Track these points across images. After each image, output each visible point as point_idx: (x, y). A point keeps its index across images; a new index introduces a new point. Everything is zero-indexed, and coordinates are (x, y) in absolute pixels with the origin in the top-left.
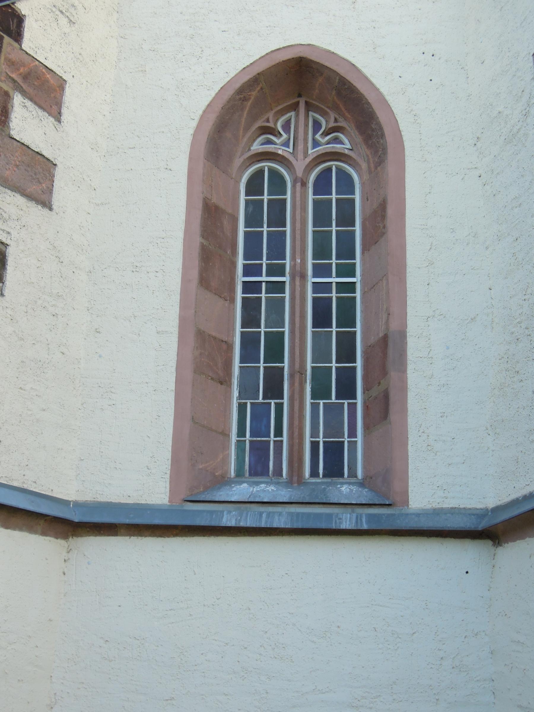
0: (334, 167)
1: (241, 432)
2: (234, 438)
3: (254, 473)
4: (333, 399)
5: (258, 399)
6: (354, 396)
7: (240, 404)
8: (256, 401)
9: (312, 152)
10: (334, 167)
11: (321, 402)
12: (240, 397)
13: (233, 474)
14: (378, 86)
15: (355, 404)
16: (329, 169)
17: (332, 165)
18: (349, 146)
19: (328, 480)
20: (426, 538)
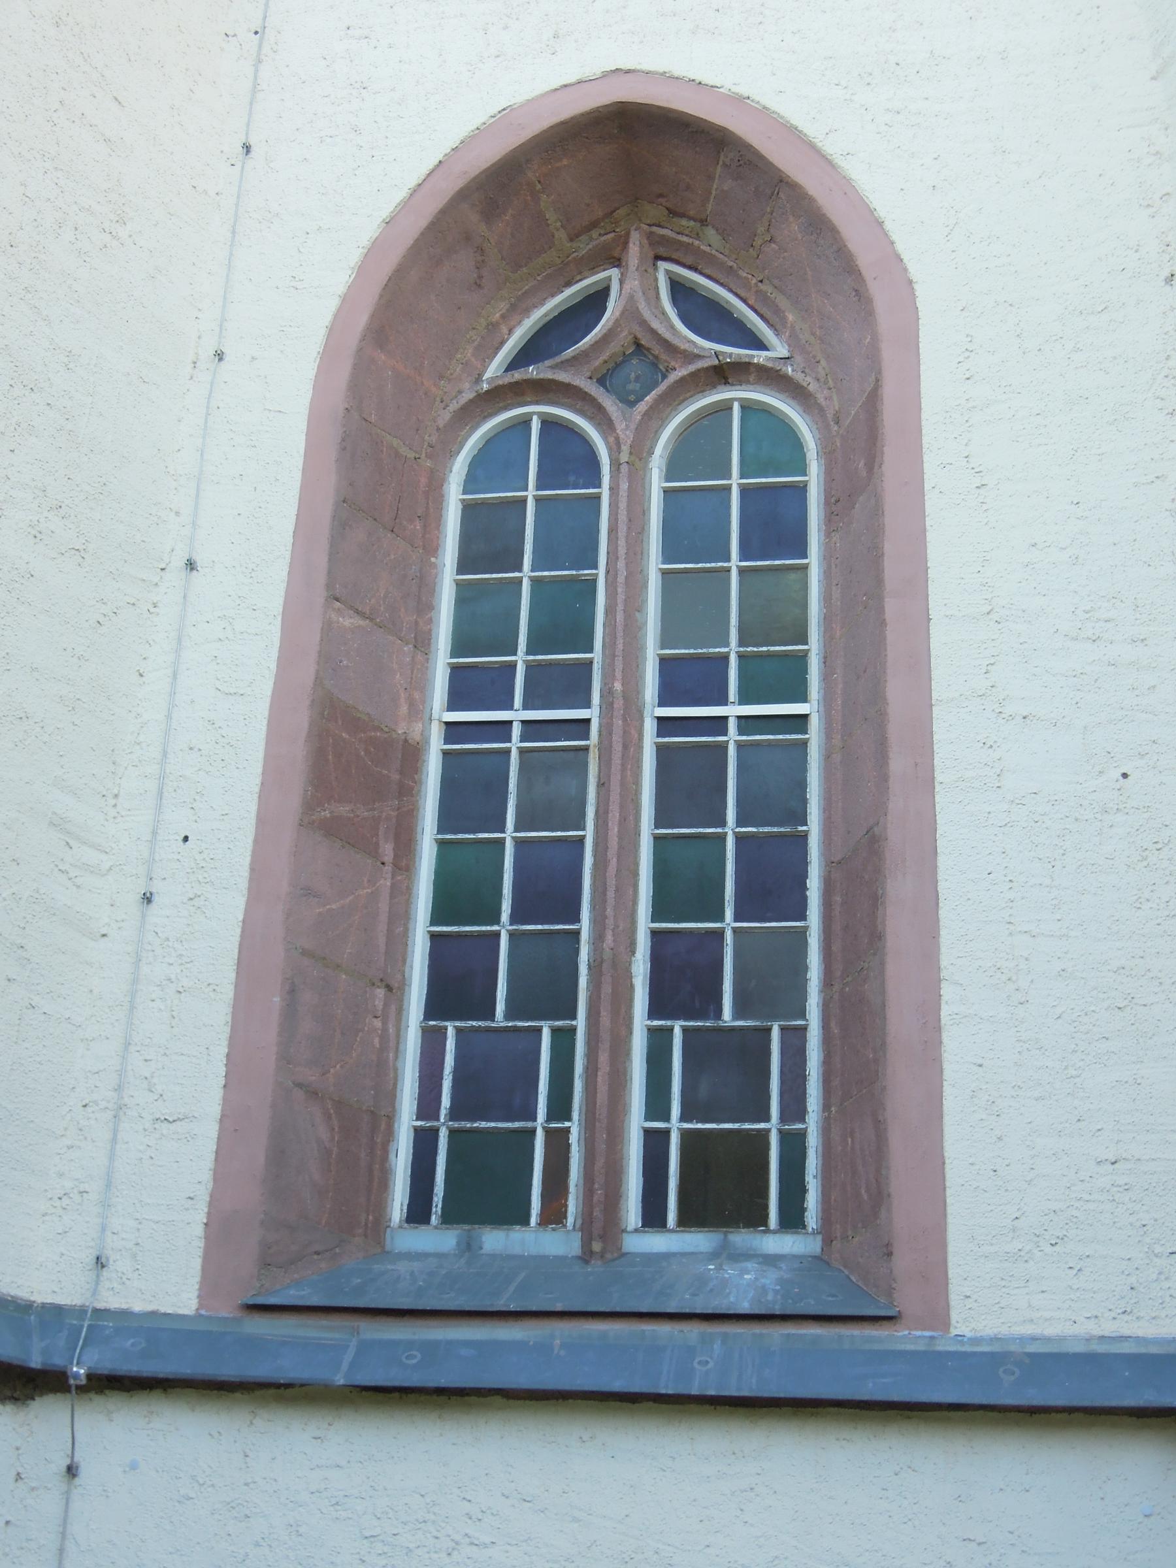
1: (427, 1105)
16: (525, 422)
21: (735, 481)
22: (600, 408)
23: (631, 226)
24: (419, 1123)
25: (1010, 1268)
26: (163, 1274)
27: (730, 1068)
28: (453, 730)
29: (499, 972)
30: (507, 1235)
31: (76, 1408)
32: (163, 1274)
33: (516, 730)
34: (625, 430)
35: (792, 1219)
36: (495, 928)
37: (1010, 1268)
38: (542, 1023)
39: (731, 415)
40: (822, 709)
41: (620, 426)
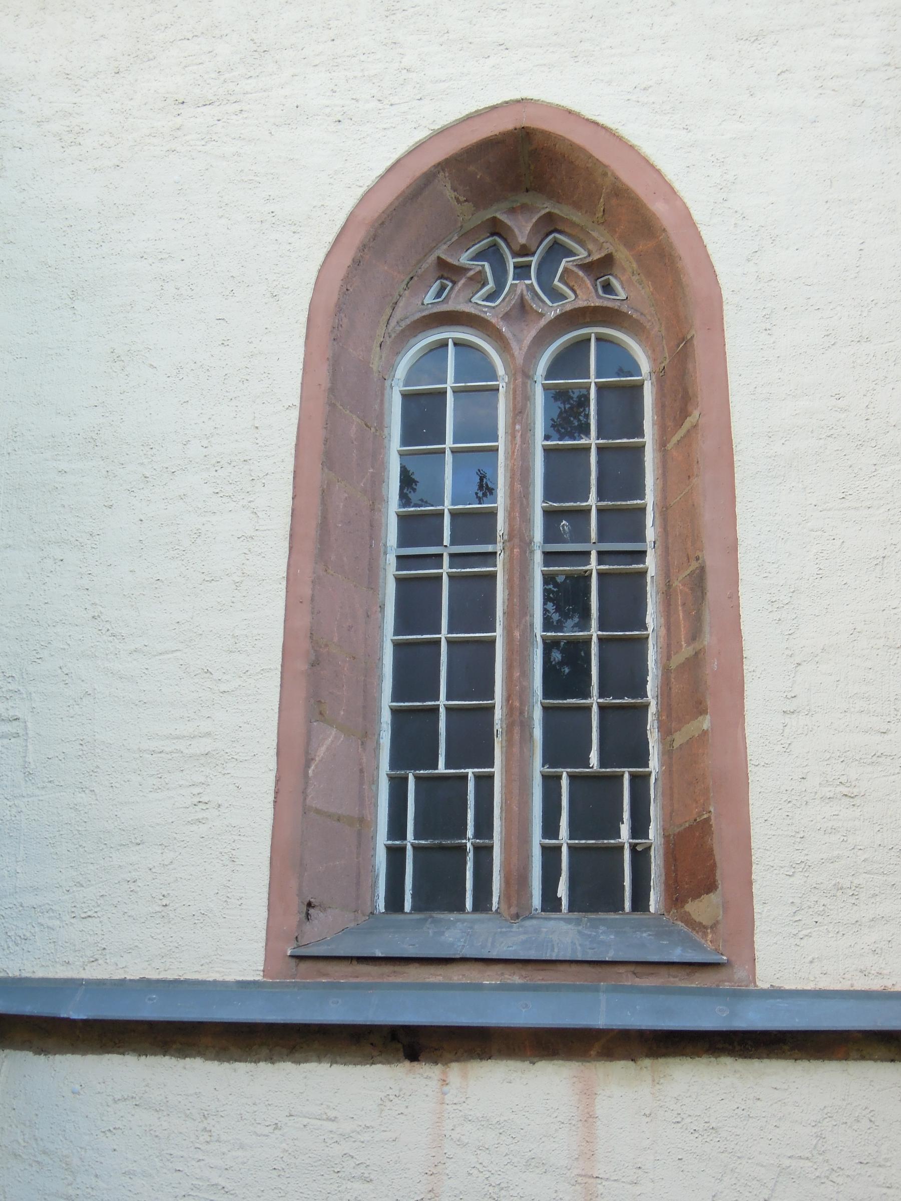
0: (593, 335)
1: (397, 827)
2: (382, 838)
3: (423, 903)
4: (442, 769)
5: (436, 768)
6: (642, 758)
7: (546, 778)
8: (436, 771)
9: (553, 310)
10: (593, 335)
11: (470, 772)
12: (395, 763)
13: (381, 906)
14: (634, 141)
15: (491, 777)
17: (591, 334)
18: (623, 295)
19: (576, 915)
20: (688, 1058)
21: (594, 700)
22: (499, 331)
23: (520, 199)
24: (390, 842)
25: (800, 942)
26: (218, 932)
27: (595, 805)
28: (403, 561)
29: (439, 740)
30: (588, 1094)
31: (602, 1107)
32: (218, 932)
33: (446, 560)
34: (519, 351)
35: (640, 901)
36: (437, 703)
37: (800, 942)
38: (467, 770)
39: (589, 347)
40: (658, 522)
41: (514, 345)
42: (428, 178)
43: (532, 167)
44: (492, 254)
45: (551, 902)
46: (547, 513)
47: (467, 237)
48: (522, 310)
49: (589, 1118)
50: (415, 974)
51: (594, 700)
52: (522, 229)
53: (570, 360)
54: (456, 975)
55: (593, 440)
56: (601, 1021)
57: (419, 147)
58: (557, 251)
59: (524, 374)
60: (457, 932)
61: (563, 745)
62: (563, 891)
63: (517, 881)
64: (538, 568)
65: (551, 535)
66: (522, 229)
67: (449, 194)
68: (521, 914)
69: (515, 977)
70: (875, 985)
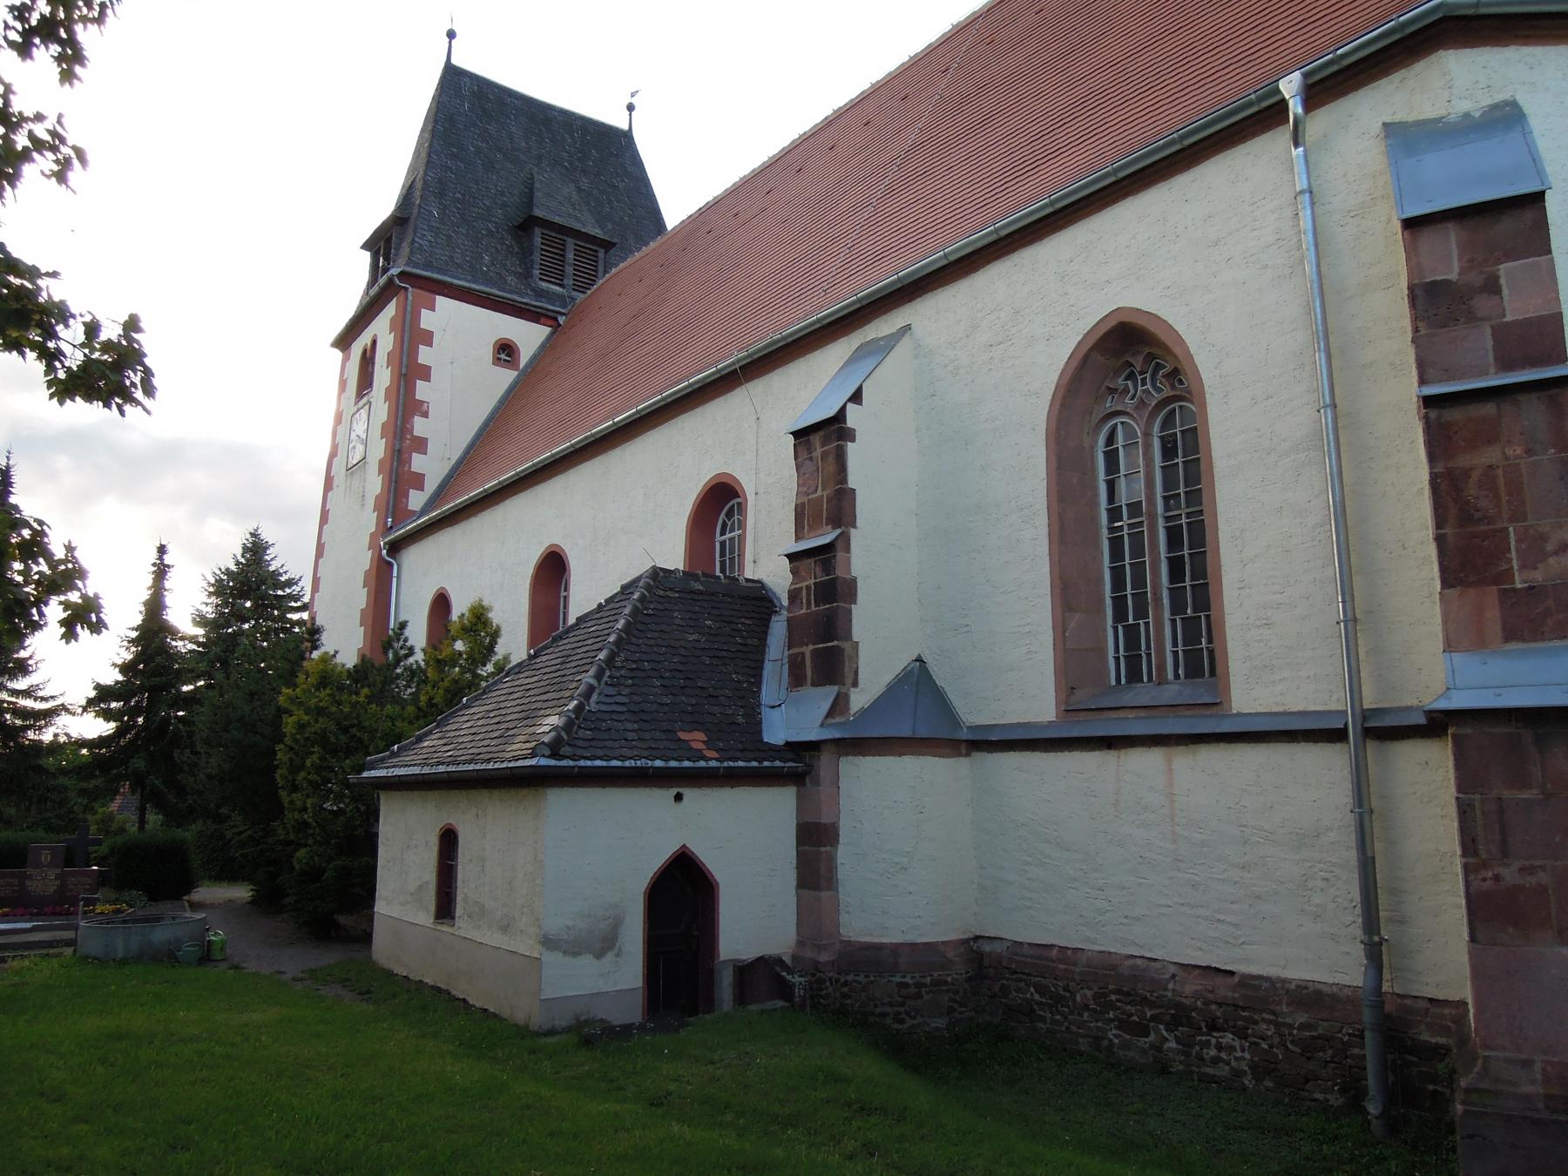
4: (1131, 621)
9: (1158, 397)
26: (1037, 702)
29: (1129, 609)
34: (1143, 423)
42: (1086, 358)
43: (363, 808)
44: (1131, 376)
45: (1177, 676)
46: (1165, 498)
47: (1117, 373)
48: (1142, 403)
49: (1170, 770)
50: (1113, 715)
51: (1188, 582)
52: (1138, 363)
53: (1168, 422)
54: (1122, 714)
55: (1180, 460)
56: (1166, 731)
57: (1080, 343)
58: (1158, 367)
59: (1147, 435)
60: (1143, 694)
61: (1178, 607)
62: (1180, 672)
63: (1162, 668)
64: (1161, 523)
65: (1167, 508)
66: (1138, 363)
67: (1101, 358)
68: (1162, 681)
69: (1143, 713)
70: (1281, 709)
